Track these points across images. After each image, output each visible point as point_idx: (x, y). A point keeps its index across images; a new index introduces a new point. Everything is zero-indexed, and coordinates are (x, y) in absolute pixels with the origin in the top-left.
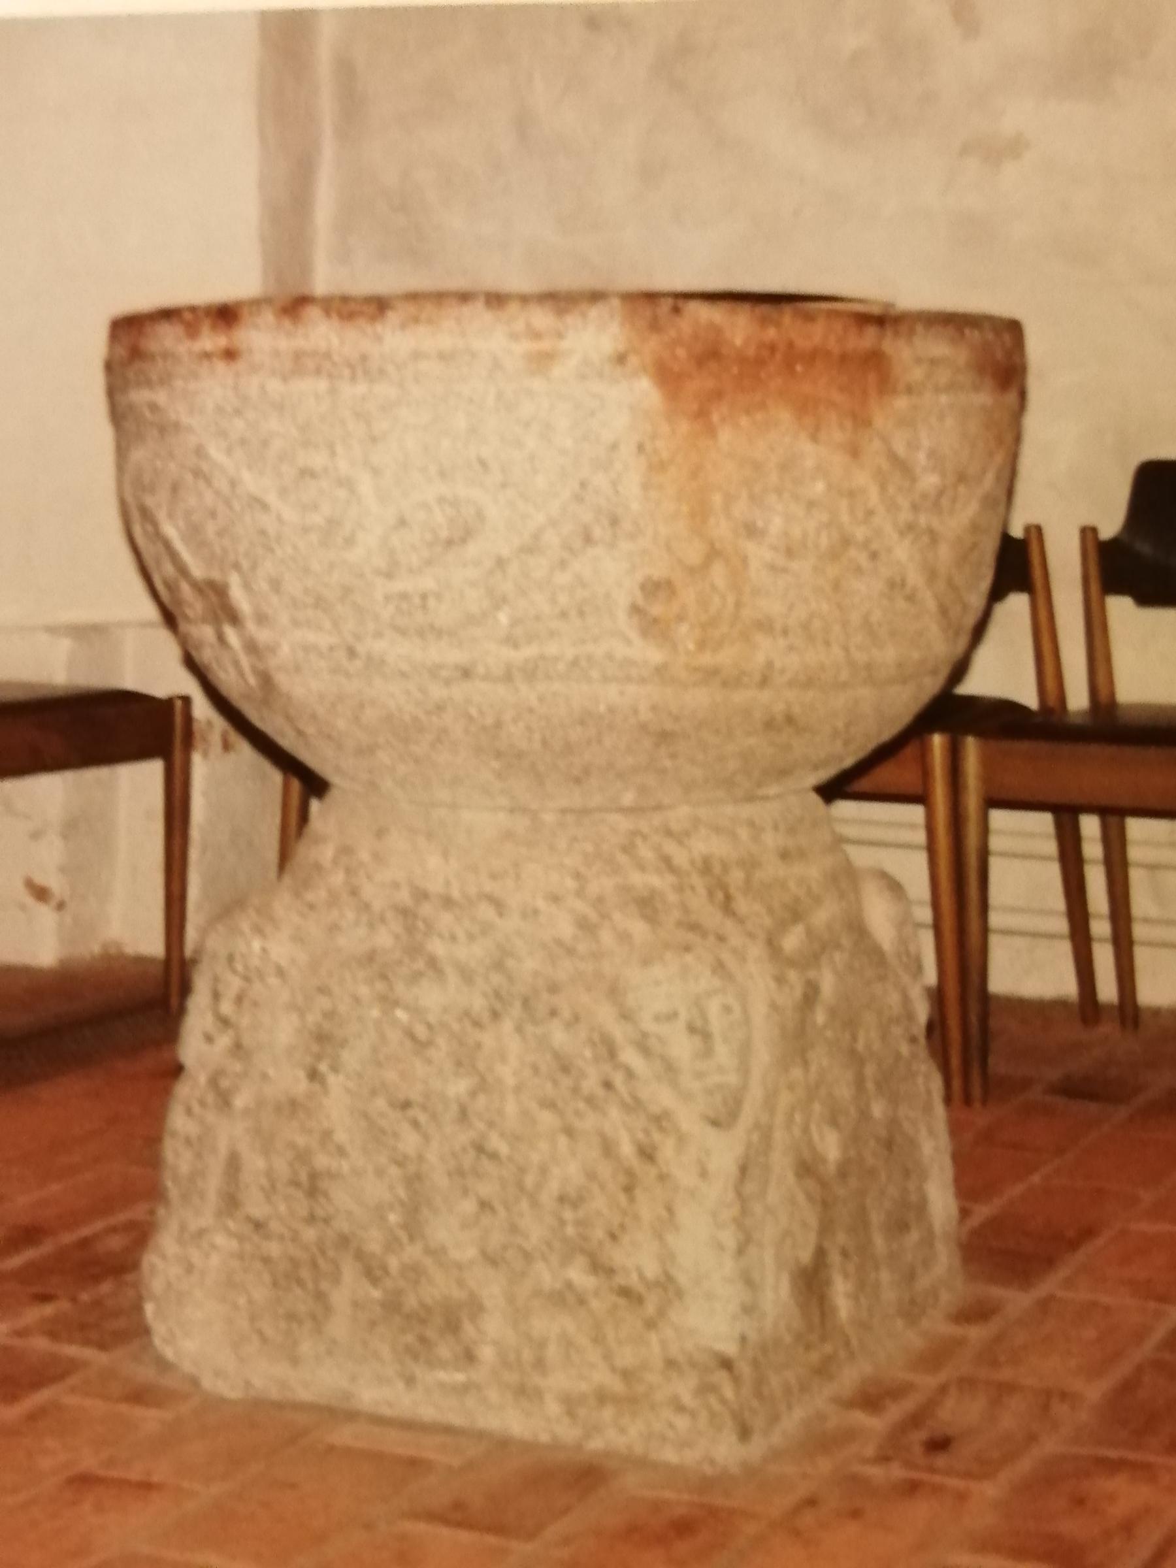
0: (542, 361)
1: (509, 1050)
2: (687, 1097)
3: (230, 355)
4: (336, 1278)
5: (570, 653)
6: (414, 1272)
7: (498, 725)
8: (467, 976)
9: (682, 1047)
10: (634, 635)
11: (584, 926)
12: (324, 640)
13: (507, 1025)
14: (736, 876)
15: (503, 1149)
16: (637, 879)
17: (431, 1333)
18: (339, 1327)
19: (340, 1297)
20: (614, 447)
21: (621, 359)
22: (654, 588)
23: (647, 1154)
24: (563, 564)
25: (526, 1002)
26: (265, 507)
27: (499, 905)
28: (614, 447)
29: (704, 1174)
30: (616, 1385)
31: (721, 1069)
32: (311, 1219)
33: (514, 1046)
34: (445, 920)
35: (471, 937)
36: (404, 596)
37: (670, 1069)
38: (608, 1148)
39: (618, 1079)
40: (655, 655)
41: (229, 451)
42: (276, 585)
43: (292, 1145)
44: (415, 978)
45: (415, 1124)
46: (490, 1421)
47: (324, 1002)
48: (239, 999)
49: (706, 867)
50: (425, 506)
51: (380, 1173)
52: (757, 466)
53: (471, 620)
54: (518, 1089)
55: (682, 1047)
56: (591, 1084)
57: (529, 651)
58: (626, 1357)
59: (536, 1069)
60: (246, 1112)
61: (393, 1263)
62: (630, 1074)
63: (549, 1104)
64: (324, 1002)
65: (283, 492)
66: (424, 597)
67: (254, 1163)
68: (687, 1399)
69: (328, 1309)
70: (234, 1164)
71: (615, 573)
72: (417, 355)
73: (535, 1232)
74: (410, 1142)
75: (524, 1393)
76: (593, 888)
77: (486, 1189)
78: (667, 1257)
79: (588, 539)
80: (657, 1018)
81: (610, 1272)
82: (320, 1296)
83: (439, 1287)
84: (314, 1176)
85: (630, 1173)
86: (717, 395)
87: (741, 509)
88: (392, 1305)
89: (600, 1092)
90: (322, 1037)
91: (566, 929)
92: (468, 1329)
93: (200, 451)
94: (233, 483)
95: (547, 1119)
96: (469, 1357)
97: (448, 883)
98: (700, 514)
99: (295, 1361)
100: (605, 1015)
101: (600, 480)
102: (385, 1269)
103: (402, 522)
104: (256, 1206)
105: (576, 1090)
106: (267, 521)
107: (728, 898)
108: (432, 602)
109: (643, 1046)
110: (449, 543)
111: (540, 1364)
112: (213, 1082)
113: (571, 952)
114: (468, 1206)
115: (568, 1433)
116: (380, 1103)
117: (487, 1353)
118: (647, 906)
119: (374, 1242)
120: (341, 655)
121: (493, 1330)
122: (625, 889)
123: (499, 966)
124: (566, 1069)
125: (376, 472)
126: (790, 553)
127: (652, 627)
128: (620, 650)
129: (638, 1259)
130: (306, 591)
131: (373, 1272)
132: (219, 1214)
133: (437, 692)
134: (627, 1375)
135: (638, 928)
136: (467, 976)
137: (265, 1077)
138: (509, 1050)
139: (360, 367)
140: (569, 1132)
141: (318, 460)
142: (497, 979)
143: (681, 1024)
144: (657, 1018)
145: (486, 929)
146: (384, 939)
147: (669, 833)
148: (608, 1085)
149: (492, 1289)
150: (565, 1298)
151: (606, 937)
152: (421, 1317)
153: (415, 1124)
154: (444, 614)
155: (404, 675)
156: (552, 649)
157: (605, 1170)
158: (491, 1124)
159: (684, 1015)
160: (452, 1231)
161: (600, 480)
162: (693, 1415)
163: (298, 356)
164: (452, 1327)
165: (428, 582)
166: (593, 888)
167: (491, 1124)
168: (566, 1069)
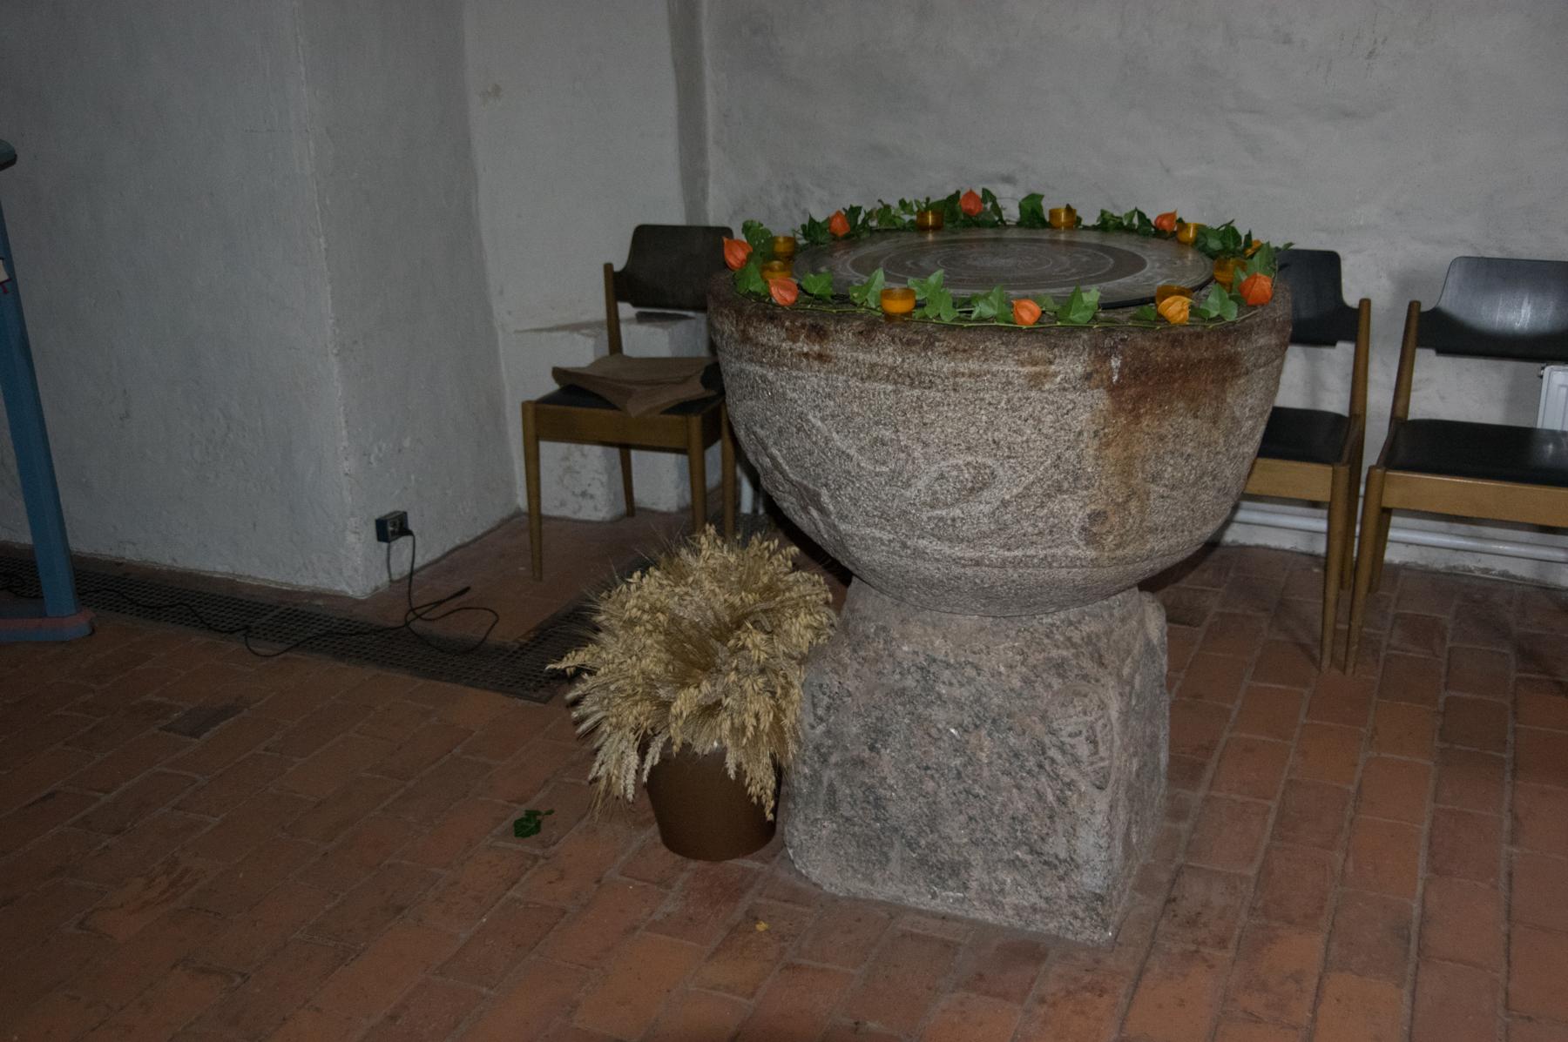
0: (1036, 381)
1: (986, 746)
2: (1085, 775)
3: (821, 357)
4: (892, 845)
5: (1042, 554)
6: (934, 848)
7: (992, 587)
8: (960, 706)
9: (1084, 750)
10: (1081, 543)
11: (1026, 681)
12: (886, 536)
13: (984, 732)
14: (1102, 644)
15: (982, 793)
16: (1054, 653)
17: (945, 875)
18: (895, 867)
19: (894, 854)
20: (1080, 433)
21: (1088, 377)
22: (1095, 517)
23: (1062, 801)
24: (1042, 506)
25: (994, 721)
26: (849, 457)
27: (977, 668)
28: (1080, 433)
29: (1093, 812)
30: (1043, 905)
31: (1102, 759)
32: (877, 819)
33: (987, 743)
34: (947, 674)
35: (962, 685)
36: (941, 519)
37: (1076, 761)
38: (1040, 796)
39: (1047, 764)
40: (1091, 553)
41: (823, 419)
42: (855, 501)
43: (863, 783)
44: (928, 705)
45: (932, 777)
46: (978, 915)
47: (878, 713)
48: (828, 708)
49: (1089, 640)
50: (957, 467)
51: (913, 800)
52: (1162, 438)
53: (984, 535)
54: (990, 763)
55: (1084, 750)
56: (1031, 763)
57: (1019, 553)
58: (1047, 892)
59: (1000, 757)
60: (836, 764)
61: (923, 842)
62: (1053, 761)
63: (1006, 773)
64: (878, 713)
65: (861, 450)
66: (953, 520)
67: (844, 790)
68: (1081, 914)
69: (888, 860)
70: (832, 790)
71: (1074, 510)
72: (955, 374)
73: (1000, 835)
74: (930, 786)
75: (995, 905)
76: (1031, 661)
77: (972, 812)
78: (1072, 850)
79: (1060, 490)
80: (1070, 735)
81: (1040, 854)
82: (885, 854)
83: (946, 855)
84: (877, 799)
85: (1052, 809)
86: (1142, 397)
87: (1151, 467)
88: (923, 861)
89: (1036, 769)
90: (878, 731)
91: (1016, 683)
92: (964, 875)
93: (801, 416)
94: (827, 440)
95: (1005, 780)
96: (966, 888)
97: (947, 655)
98: (1126, 472)
99: (873, 883)
100: (1039, 728)
101: (1070, 455)
102: (918, 843)
103: (942, 476)
104: (846, 810)
105: (1022, 767)
106: (849, 466)
107: (1100, 656)
108: (958, 524)
109: (1061, 748)
110: (972, 489)
111: (1002, 891)
112: (817, 748)
113: (1020, 695)
114: (963, 818)
115: (1018, 923)
116: (912, 766)
117: (974, 885)
118: (1060, 667)
119: (911, 831)
120: (897, 546)
121: (978, 874)
122: (1050, 659)
123: (978, 700)
124: (1016, 755)
125: (926, 445)
126: (1173, 488)
127: (1092, 539)
128: (1072, 552)
129: (1057, 846)
130: (876, 508)
131: (911, 845)
132: (825, 812)
133: (957, 570)
134: (1047, 900)
135: (1056, 683)
136: (960, 706)
137: (846, 749)
138: (986, 746)
139: (915, 379)
140: (1019, 787)
141: (888, 434)
142: (977, 708)
143: (1082, 738)
144: (1070, 735)
145: (971, 681)
146: (910, 682)
147: (1071, 623)
148: (1041, 766)
149: (976, 857)
150: (1013, 864)
151: (1039, 688)
152: (941, 866)
153: (932, 777)
154: (966, 530)
155: (937, 560)
156: (1031, 552)
157: (1038, 807)
158: (975, 781)
159: (1085, 733)
160: (955, 829)
161: (1070, 455)
162: (1083, 920)
163: (873, 366)
164: (955, 873)
165: (957, 512)
166: (1031, 661)
167: (975, 781)
168: (1016, 755)
